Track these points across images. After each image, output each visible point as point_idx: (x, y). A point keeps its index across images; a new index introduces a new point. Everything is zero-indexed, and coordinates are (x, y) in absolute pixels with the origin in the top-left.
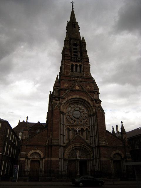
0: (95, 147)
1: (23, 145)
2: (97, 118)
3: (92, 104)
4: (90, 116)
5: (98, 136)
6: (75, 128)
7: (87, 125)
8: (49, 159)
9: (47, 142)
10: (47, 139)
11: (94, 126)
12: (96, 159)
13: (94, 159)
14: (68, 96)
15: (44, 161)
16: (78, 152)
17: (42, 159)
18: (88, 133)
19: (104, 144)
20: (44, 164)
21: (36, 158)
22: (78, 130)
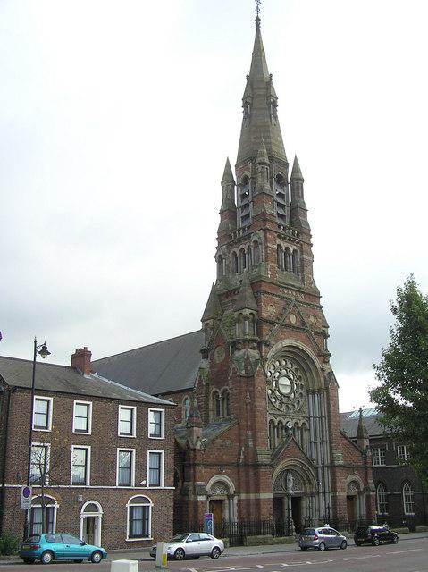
0: (323, 467)
1: (199, 465)
2: (328, 400)
3: (319, 366)
4: (311, 392)
5: (331, 443)
6: (284, 422)
7: (304, 415)
8: (252, 496)
9: (242, 457)
10: (240, 449)
11: (321, 417)
12: (324, 493)
13: (318, 493)
14: (277, 340)
15: (236, 501)
16: (291, 477)
17: (230, 497)
18: (304, 433)
19: (341, 462)
20: (236, 508)
21: (219, 494)
22: (290, 427)
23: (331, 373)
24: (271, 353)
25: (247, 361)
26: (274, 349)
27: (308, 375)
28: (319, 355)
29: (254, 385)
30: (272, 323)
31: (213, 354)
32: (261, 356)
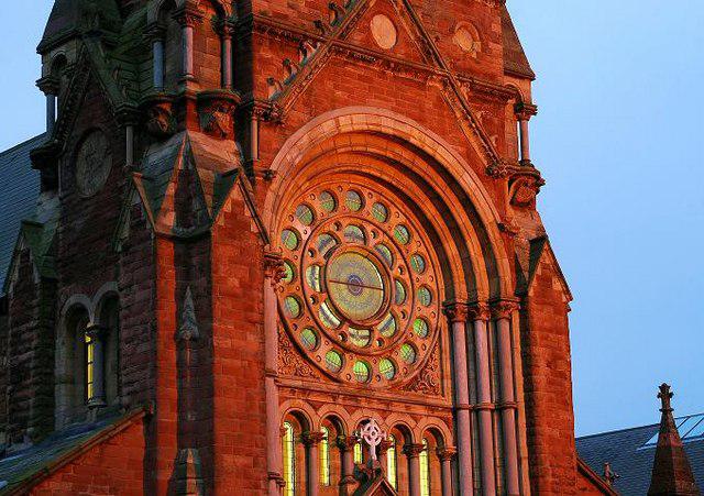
3: (488, 214)
6: (350, 422)
7: (432, 400)
11: (494, 302)
14: (315, 106)
23: (540, 242)
24: (287, 155)
25: (188, 178)
26: (302, 137)
27: (451, 249)
28: (489, 176)
29: (207, 269)
30: (294, 41)
31: (73, 168)
32: (248, 164)
